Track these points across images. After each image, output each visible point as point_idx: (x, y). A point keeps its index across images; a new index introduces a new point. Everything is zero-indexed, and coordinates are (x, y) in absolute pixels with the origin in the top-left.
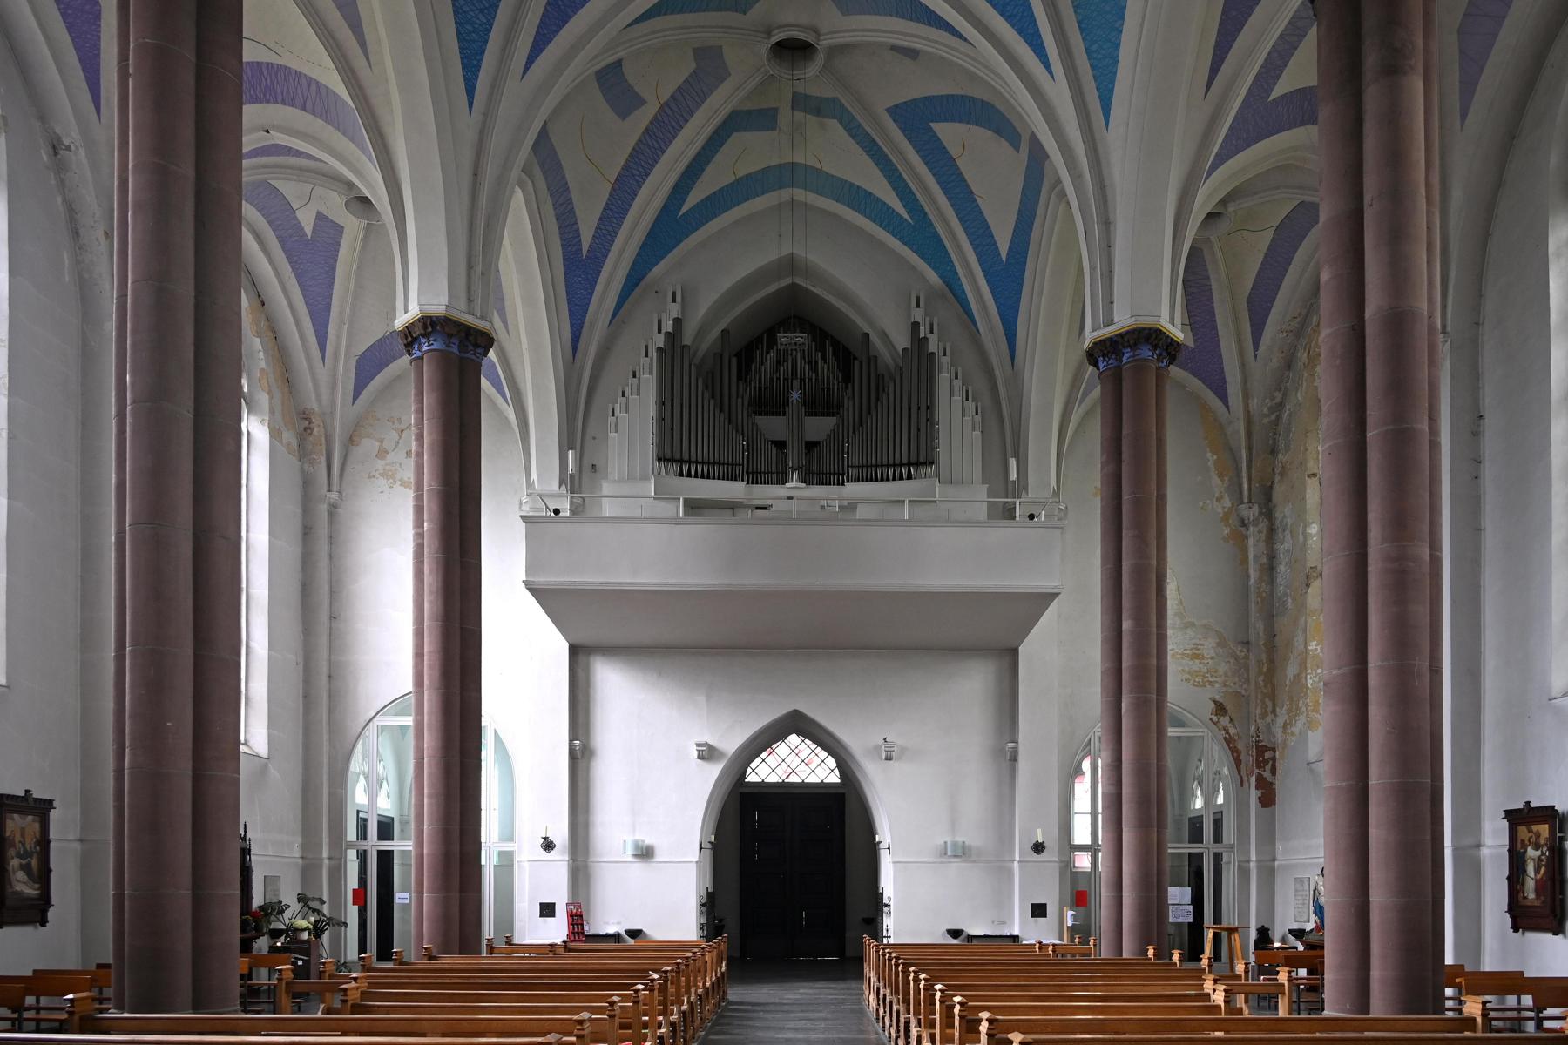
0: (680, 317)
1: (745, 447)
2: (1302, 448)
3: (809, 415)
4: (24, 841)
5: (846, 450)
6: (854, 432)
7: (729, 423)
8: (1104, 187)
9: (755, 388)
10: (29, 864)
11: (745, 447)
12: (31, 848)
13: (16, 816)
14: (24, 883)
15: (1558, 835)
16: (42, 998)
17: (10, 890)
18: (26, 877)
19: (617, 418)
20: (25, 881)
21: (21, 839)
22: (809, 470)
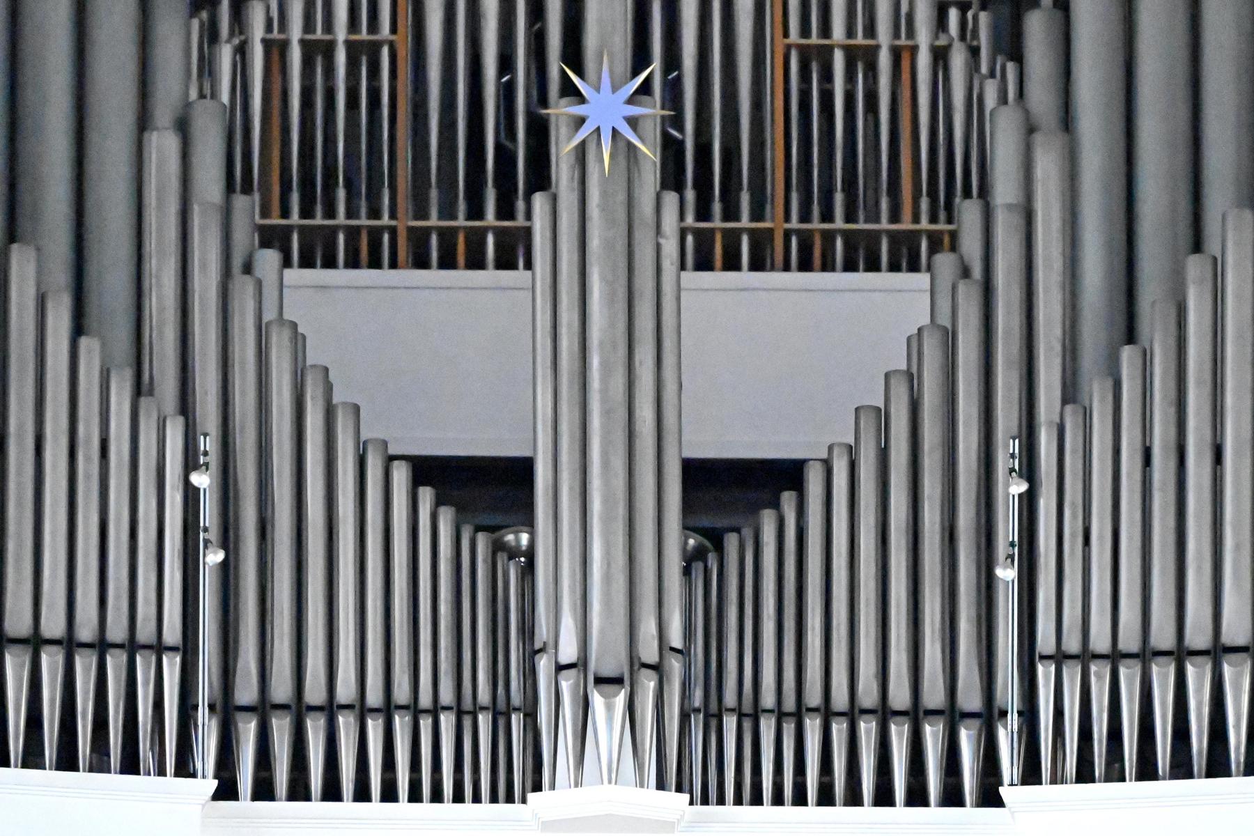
1: (208, 514)
3: (704, 264)
5: (1008, 529)
6: (1070, 393)
9: (276, 50)
11: (208, 514)
22: (714, 680)
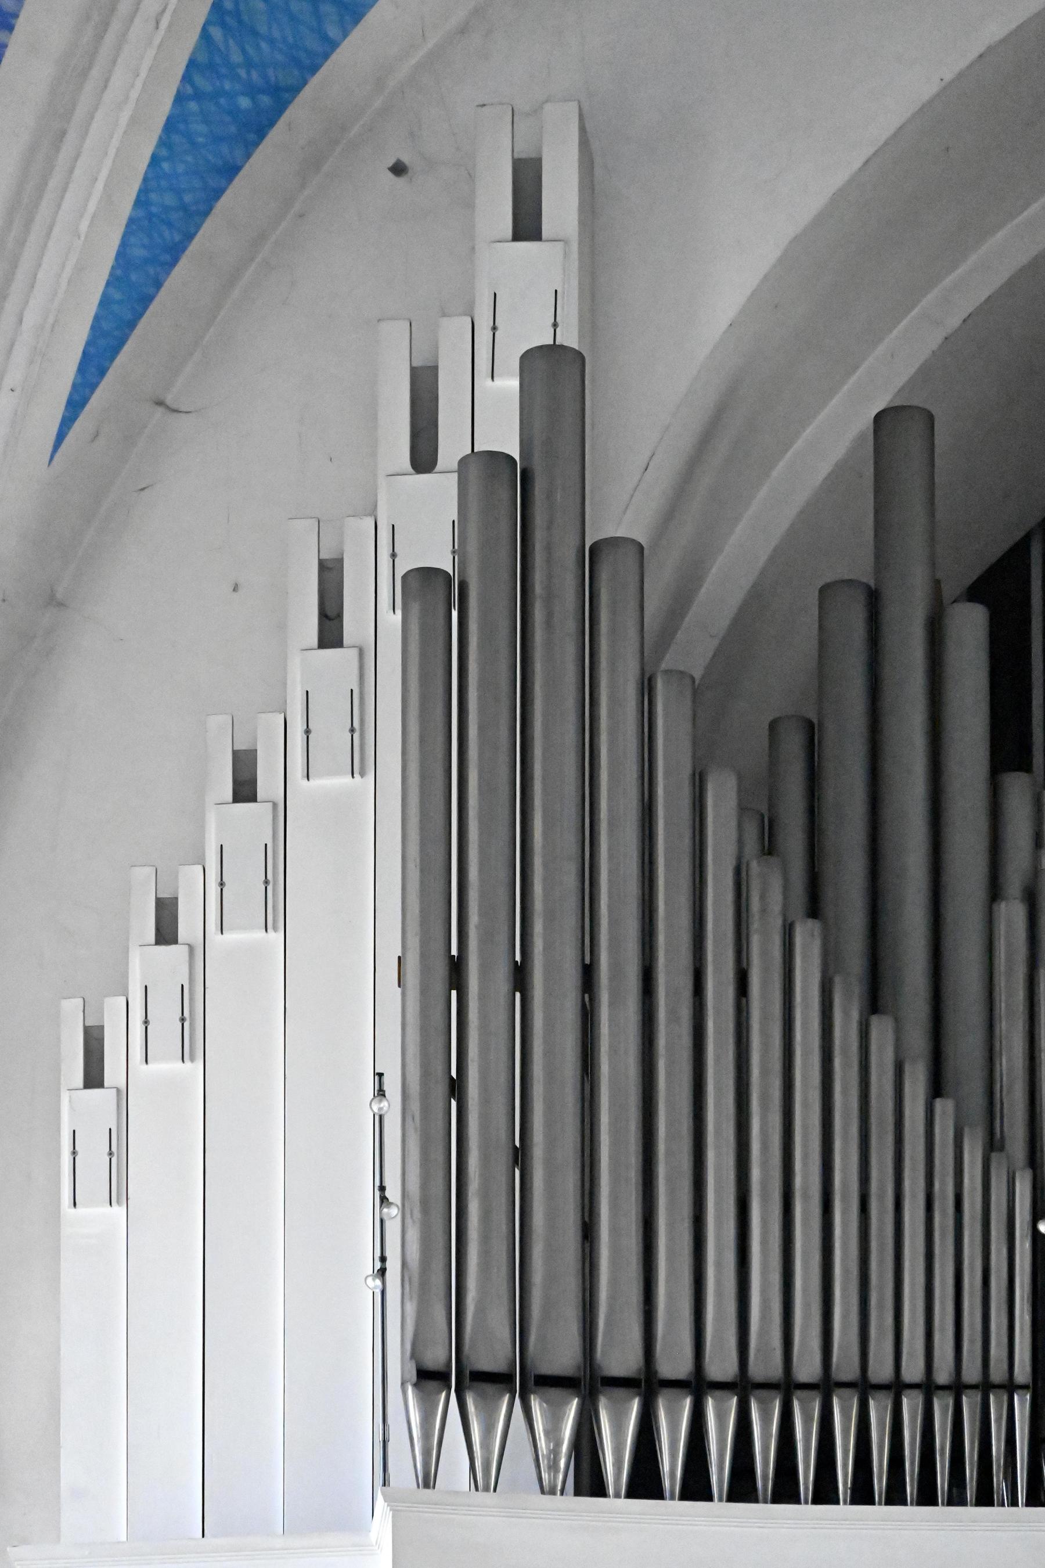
0: (569, 338)
7: (937, 1088)
19: (123, 1096)
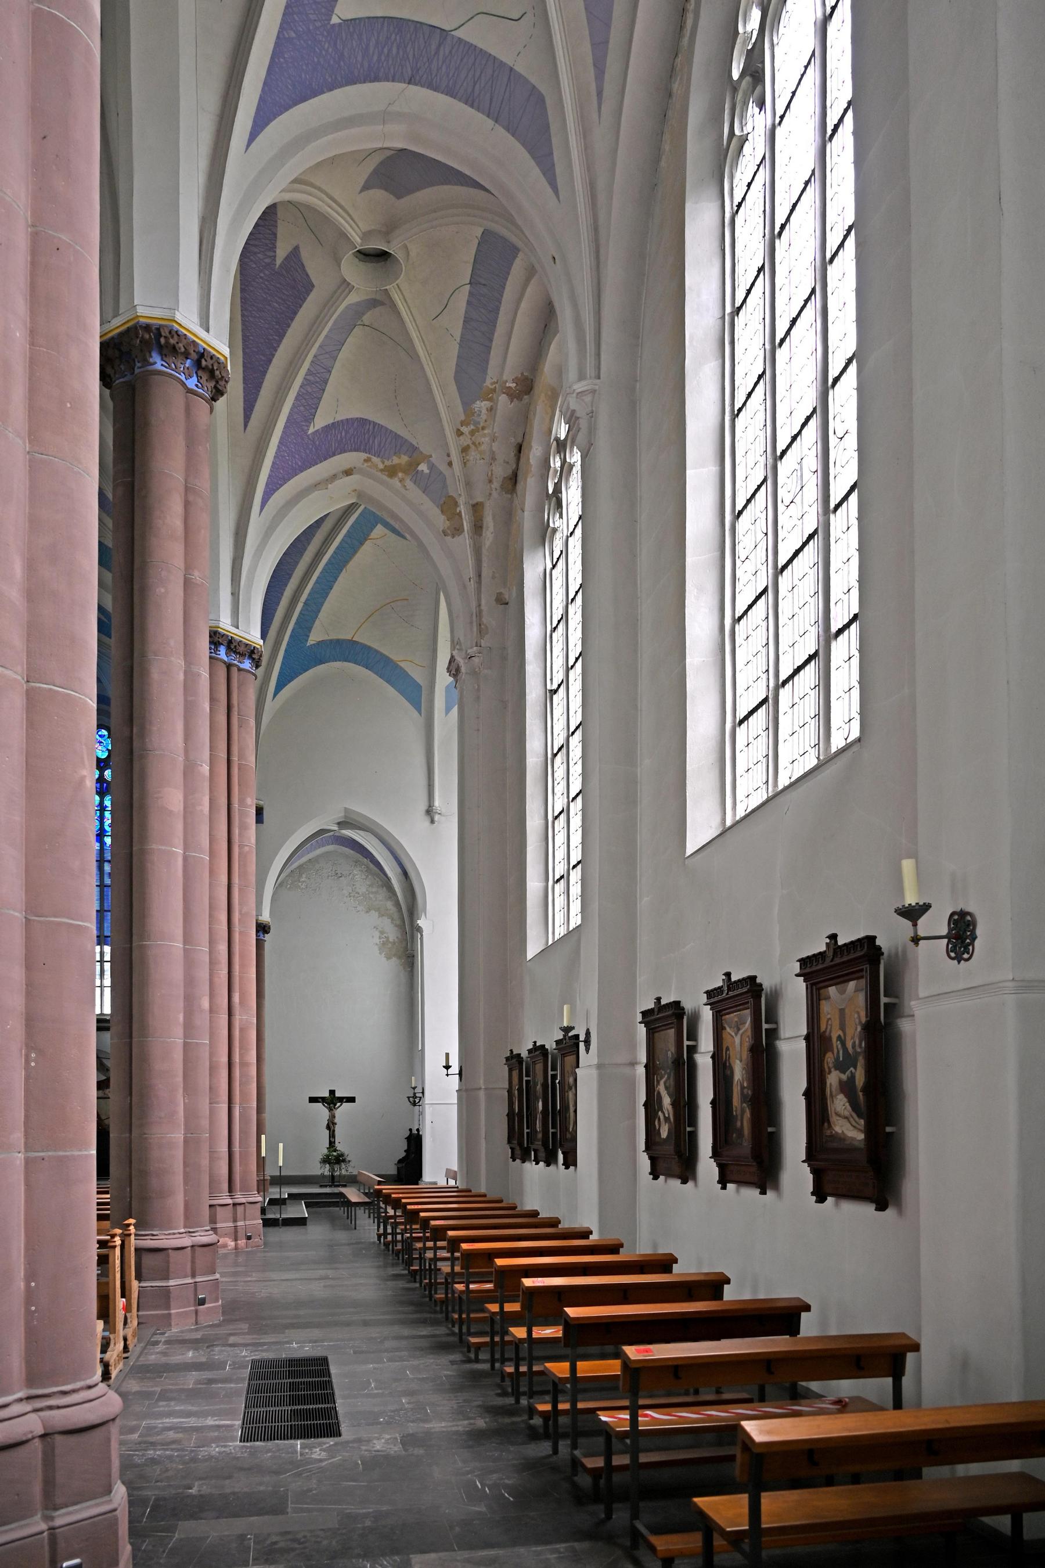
2: (108, 840)
4: (845, 1035)
8: (481, 527)
10: (852, 1078)
12: (854, 1046)
13: (832, 990)
14: (846, 1118)
15: (688, 1129)
16: (580, 1364)
17: (828, 1132)
18: (849, 1108)
20: (847, 1113)
21: (840, 1033)
